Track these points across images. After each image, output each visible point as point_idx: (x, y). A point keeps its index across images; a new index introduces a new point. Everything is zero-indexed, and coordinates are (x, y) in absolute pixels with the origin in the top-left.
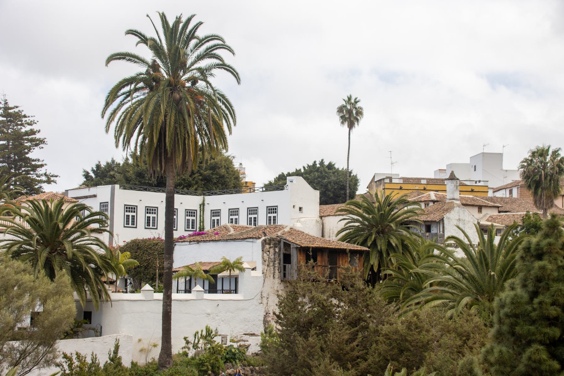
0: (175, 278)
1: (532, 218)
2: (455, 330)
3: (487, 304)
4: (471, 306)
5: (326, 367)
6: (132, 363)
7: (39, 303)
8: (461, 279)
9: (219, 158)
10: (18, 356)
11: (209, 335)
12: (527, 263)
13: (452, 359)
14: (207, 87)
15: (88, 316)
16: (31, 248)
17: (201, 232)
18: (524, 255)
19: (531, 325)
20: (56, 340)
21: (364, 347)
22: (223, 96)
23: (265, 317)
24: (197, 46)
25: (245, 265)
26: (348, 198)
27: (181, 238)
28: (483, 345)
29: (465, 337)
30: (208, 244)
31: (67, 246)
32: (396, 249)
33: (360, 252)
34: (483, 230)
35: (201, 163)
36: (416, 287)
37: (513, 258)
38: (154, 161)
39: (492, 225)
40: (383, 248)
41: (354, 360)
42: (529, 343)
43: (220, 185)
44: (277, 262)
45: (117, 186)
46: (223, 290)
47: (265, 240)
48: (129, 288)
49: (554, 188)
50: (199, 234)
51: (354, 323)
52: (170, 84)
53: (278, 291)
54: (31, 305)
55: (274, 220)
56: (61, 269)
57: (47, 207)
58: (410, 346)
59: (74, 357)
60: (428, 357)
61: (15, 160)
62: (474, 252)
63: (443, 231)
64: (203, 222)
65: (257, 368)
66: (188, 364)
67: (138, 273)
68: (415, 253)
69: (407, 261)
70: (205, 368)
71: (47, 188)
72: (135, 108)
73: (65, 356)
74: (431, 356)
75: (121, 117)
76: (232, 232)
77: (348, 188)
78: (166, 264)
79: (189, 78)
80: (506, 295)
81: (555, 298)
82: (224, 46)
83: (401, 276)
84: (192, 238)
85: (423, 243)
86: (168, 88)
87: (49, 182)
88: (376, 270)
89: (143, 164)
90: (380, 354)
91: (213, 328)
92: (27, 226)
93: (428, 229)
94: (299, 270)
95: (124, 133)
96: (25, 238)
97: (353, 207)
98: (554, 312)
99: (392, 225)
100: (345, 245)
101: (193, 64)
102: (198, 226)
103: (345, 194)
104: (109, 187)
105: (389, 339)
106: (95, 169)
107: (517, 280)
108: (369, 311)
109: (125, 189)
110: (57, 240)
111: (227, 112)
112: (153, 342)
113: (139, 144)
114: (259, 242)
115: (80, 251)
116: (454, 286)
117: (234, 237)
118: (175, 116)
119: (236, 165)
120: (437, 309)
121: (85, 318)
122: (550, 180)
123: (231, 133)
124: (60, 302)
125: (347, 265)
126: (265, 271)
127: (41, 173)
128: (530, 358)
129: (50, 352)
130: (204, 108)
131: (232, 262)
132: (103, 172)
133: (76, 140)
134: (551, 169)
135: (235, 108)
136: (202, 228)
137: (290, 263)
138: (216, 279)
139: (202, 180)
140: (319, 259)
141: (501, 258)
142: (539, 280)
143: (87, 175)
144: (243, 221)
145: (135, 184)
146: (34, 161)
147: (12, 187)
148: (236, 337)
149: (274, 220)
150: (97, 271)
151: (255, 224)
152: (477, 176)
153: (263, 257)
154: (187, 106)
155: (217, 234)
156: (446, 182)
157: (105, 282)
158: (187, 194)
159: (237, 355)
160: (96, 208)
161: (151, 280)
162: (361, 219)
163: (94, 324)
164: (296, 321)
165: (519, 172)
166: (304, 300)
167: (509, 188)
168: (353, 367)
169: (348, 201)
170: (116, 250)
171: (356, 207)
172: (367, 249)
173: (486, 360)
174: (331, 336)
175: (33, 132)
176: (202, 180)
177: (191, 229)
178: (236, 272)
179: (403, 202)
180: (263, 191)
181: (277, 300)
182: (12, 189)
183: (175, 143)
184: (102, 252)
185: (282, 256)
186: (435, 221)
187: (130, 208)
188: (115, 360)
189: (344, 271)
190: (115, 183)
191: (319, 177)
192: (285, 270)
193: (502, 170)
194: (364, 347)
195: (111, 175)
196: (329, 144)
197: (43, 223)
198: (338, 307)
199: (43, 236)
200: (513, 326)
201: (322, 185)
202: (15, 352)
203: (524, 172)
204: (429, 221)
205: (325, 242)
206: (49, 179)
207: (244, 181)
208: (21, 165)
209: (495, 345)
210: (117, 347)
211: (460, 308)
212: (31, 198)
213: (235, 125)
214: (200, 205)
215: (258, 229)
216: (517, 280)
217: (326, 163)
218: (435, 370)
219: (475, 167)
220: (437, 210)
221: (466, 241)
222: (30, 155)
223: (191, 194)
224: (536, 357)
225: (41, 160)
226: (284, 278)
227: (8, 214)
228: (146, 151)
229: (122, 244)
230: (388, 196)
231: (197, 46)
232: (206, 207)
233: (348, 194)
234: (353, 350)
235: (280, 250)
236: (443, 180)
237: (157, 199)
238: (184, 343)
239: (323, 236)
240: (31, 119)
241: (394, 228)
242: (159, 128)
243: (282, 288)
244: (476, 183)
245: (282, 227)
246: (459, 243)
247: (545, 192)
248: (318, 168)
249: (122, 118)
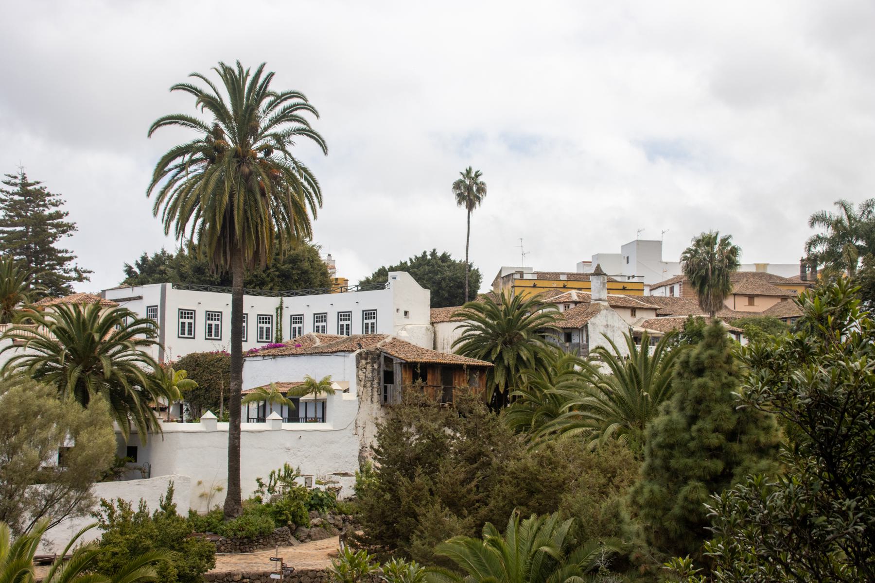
0: (245, 403)
1: (695, 324)
2: (599, 465)
3: (638, 432)
4: (619, 435)
5: (436, 515)
6: (190, 512)
7: (68, 436)
8: (608, 402)
9: (301, 248)
10: (44, 502)
11: (288, 475)
12: (685, 381)
13: (594, 501)
14: (286, 158)
15: (132, 452)
16: (58, 366)
17: (278, 344)
18: (682, 371)
19: (688, 457)
20: (92, 482)
21: (486, 489)
22: (305, 170)
23: (361, 451)
24: (272, 106)
25: (335, 386)
26: (467, 299)
27: (251, 351)
28: (632, 483)
29: (611, 474)
30: (287, 359)
31: (105, 363)
32: (528, 364)
33: (482, 369)
34: (635, 338)
35: (278, 254)
36: (552, 413)
37: (670, 374)
38: (217, 252)
39: (646, 332)
40: (511, 362)
41: (470, 505)
42: (686, 481)
43: (303, 283)
44: (376, 382)
45: (169, 285)
46: (306, 418)
47: (360, 354)
48: (185, 416)
49: (724, 285)
50: (275, 347)
51: (472, 459)
52: (236, 154)
53: (377, 419)
54: (59, 437)
55: (373, 327)
56: (97, 391)
57: (79, 313)
58: (541, 487)
59: (116, 505)
60: (564, 500)
61: (36, 252)
62: (623, 365)
63: (587, 341)
64: (281, 330)
65: (351, 517)
66: (262, 512)
67: (196, 397)
68: (550, 369)
69: (542, 379)
70: (284, 518)
71: (78, 288)
72: (192, 185)
73: (104, 503)
74: (567, 498)
75: (172, 196)
76: (318, 343)
77: (467, 286)
78: (233, 386)
79: (261, 146)
80: (659, 421)
81: (718, 422)
82: (306, 107)
83: (533, 398)
84: (266, 351)
85: (560, 356)
86: (235, 160)
87: (80, 279)
88: (502, 391)
89: (202, 257)
90: (504, 497)
91: (293, 466)
92: (53, 337)
93: (568, 338)
94: (404, 391)
95: (177, 217)
96: (50, 352)
97: (473, 311)
98: (717, 441)
99: (523, 333)
100: (463, 360)
101: (266, 129)
102: (274, 335)
103: (464, 294)
104: (159, 286)
105: (516, 478)
106: (140, 262)
107: (672, 403)
108: (493, 443)
109: (178, 288)
110: (92, 355)
111: (311, 190)
112: (216, 485)
113: (196, 231)
114: (353, 355)
115: (122, 370)
116: (599, 411)
117: (320, 350)
118: (245, 196)
119: (323, 256)
120: (577, 439)
121: (129, 455)
122: (719, 275)
123: (315, 218)
124: (96, 435)
125: (464, 385)
126: (361, 394)
127: (70, 267)
128: (686, 499)
129: (86, 498)
130: (281, 185)
131: (318, 382)
132: (150, 267)
133: (115, 227)
134: (720, 261)
135: (321, 185)
136: (279, 339)
137: (392, 383)
138: (298, 404)
139: (278, 276)
140: (429, 377)
141: (657, 374)
142: (699, 401)
143: (129, 271)
144: (332, 330)
145: (193, 282)
146: (60, 252)
147: (32, 286)
148: (324, 478)
149: (373, 327)
150: (144, 395)
151: (348, 334)
152: (630, 270)
153: (358, 376)
154: (259, 183)
155: (299, 346)
156: (591, 278)
157: (154, 409)
158: (260, 294)
159: (325, 501)
160: (142, 315)
161: (214, 406)
162: (483, 326)
163: (140, 463)
164: (401, 456)
165: (682, 264)
166: (410, 430)
167: (670, 284)
168: (470, 513)
169: (467, 303)
170: (168, 368)
171: (477, 310)
172: (491, 364)
173: (634, 502)
174: (441, 476)
175: (59, 215)
176: (278, 276)
177: (264, 340)
178: (324, 395)
179: (536, 304)
180: (358, 291)
181: (375, 431)
182: (32, 290)
183: (246, 228)
184: (150, 370)
185: (382, 374)
186: (577, 328)
187: (186, 314)
188: (168, 508)
189: (460, 394)
190: (167, 281)
191: (430, 272)
192: (386, 391)
193: (661, 262)
194: (486, 489)
195: (161, 271)
196: (441, 228)
197: (74, 332)
198: (453, 438)
199: (73, 350)
200: (666, 459)
201: (434, 283)
202: (40, 498)
203: (687, 265)
204: (569, 328)
205: (438, 355)
206: (80, 275)
207: (333, 277)
208: (44, 257)
209: (645, 483)
210: (171, 492)
211: (606, 436)
212: (57, 301)
213: (321, 206)
214: (277, 309)
215: (352, 339)
216: (672, 403)
217: (439, 254)
218: (573, 515)
220: (580, 314)
221: (613, 353)
222: (56, 245)
223: (264, 295)
224: (694, 496)
225: (70, 250)
226: (385, 402)
227: (28, 322)
228: (206, 239)
229: (176, 360)
230: (517, 297)
231: (272, 106)
232: (285, 311)
233: (467, 294)
234: (469, 492)
235: (379, 367)
236: (587, 275)
237: (222, 301)
238: (256, 486)
239: (435, 348)
240: (57, 198)
241: (525, 337)
242: (223, 211)
243: (383, 415)
244: (629, 278)
245: (382, 337)
246: (605, 356)
247: (713, 290)
248: (429, 260)
249: (174, 197)
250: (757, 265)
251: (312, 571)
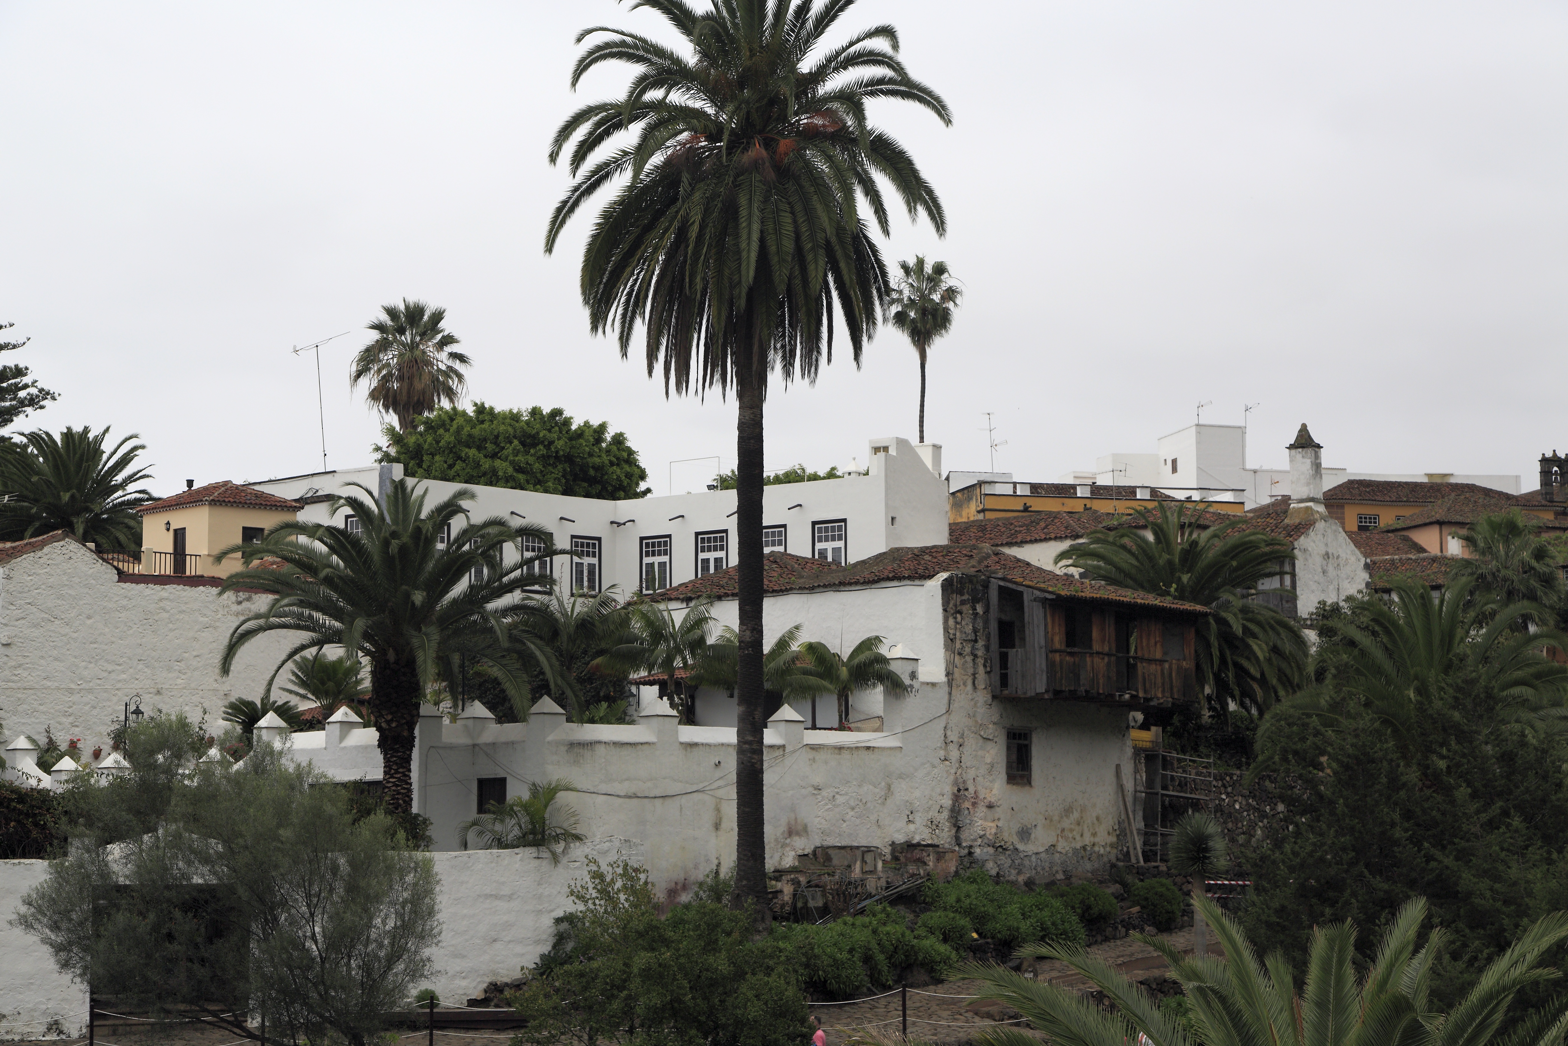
44: (981, 643)
114: (935, 585)
143: (920, 262)
185: (994, 626)
219: (1174, 462)
235: (987, 611)
250: (1430, 476)
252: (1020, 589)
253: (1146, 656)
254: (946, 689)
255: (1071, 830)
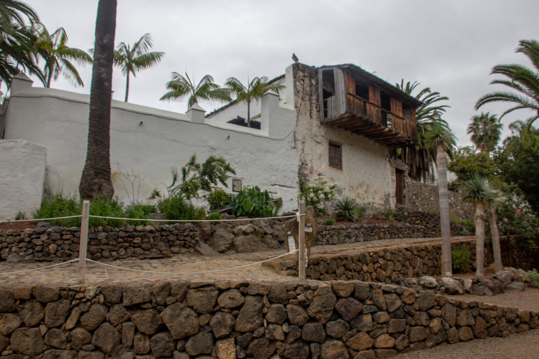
44: (314, 97)
126: (299, 106)
235: (317, 83)
243: (323, 133)
251: (200, 287)
252: (332, 68)
253: (395, 114)
254: (296, 114)
255: (363, 194)
